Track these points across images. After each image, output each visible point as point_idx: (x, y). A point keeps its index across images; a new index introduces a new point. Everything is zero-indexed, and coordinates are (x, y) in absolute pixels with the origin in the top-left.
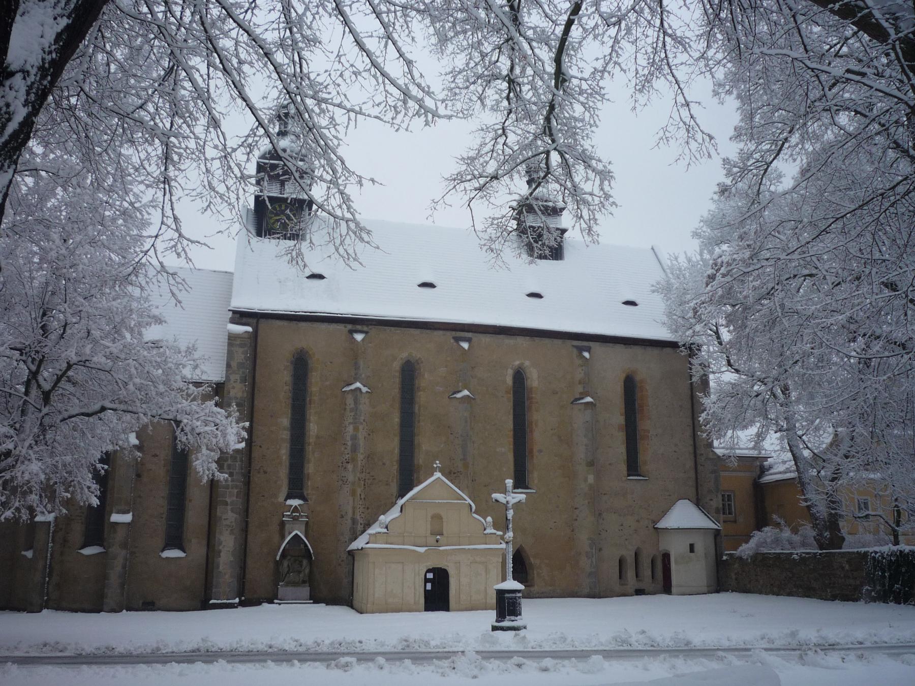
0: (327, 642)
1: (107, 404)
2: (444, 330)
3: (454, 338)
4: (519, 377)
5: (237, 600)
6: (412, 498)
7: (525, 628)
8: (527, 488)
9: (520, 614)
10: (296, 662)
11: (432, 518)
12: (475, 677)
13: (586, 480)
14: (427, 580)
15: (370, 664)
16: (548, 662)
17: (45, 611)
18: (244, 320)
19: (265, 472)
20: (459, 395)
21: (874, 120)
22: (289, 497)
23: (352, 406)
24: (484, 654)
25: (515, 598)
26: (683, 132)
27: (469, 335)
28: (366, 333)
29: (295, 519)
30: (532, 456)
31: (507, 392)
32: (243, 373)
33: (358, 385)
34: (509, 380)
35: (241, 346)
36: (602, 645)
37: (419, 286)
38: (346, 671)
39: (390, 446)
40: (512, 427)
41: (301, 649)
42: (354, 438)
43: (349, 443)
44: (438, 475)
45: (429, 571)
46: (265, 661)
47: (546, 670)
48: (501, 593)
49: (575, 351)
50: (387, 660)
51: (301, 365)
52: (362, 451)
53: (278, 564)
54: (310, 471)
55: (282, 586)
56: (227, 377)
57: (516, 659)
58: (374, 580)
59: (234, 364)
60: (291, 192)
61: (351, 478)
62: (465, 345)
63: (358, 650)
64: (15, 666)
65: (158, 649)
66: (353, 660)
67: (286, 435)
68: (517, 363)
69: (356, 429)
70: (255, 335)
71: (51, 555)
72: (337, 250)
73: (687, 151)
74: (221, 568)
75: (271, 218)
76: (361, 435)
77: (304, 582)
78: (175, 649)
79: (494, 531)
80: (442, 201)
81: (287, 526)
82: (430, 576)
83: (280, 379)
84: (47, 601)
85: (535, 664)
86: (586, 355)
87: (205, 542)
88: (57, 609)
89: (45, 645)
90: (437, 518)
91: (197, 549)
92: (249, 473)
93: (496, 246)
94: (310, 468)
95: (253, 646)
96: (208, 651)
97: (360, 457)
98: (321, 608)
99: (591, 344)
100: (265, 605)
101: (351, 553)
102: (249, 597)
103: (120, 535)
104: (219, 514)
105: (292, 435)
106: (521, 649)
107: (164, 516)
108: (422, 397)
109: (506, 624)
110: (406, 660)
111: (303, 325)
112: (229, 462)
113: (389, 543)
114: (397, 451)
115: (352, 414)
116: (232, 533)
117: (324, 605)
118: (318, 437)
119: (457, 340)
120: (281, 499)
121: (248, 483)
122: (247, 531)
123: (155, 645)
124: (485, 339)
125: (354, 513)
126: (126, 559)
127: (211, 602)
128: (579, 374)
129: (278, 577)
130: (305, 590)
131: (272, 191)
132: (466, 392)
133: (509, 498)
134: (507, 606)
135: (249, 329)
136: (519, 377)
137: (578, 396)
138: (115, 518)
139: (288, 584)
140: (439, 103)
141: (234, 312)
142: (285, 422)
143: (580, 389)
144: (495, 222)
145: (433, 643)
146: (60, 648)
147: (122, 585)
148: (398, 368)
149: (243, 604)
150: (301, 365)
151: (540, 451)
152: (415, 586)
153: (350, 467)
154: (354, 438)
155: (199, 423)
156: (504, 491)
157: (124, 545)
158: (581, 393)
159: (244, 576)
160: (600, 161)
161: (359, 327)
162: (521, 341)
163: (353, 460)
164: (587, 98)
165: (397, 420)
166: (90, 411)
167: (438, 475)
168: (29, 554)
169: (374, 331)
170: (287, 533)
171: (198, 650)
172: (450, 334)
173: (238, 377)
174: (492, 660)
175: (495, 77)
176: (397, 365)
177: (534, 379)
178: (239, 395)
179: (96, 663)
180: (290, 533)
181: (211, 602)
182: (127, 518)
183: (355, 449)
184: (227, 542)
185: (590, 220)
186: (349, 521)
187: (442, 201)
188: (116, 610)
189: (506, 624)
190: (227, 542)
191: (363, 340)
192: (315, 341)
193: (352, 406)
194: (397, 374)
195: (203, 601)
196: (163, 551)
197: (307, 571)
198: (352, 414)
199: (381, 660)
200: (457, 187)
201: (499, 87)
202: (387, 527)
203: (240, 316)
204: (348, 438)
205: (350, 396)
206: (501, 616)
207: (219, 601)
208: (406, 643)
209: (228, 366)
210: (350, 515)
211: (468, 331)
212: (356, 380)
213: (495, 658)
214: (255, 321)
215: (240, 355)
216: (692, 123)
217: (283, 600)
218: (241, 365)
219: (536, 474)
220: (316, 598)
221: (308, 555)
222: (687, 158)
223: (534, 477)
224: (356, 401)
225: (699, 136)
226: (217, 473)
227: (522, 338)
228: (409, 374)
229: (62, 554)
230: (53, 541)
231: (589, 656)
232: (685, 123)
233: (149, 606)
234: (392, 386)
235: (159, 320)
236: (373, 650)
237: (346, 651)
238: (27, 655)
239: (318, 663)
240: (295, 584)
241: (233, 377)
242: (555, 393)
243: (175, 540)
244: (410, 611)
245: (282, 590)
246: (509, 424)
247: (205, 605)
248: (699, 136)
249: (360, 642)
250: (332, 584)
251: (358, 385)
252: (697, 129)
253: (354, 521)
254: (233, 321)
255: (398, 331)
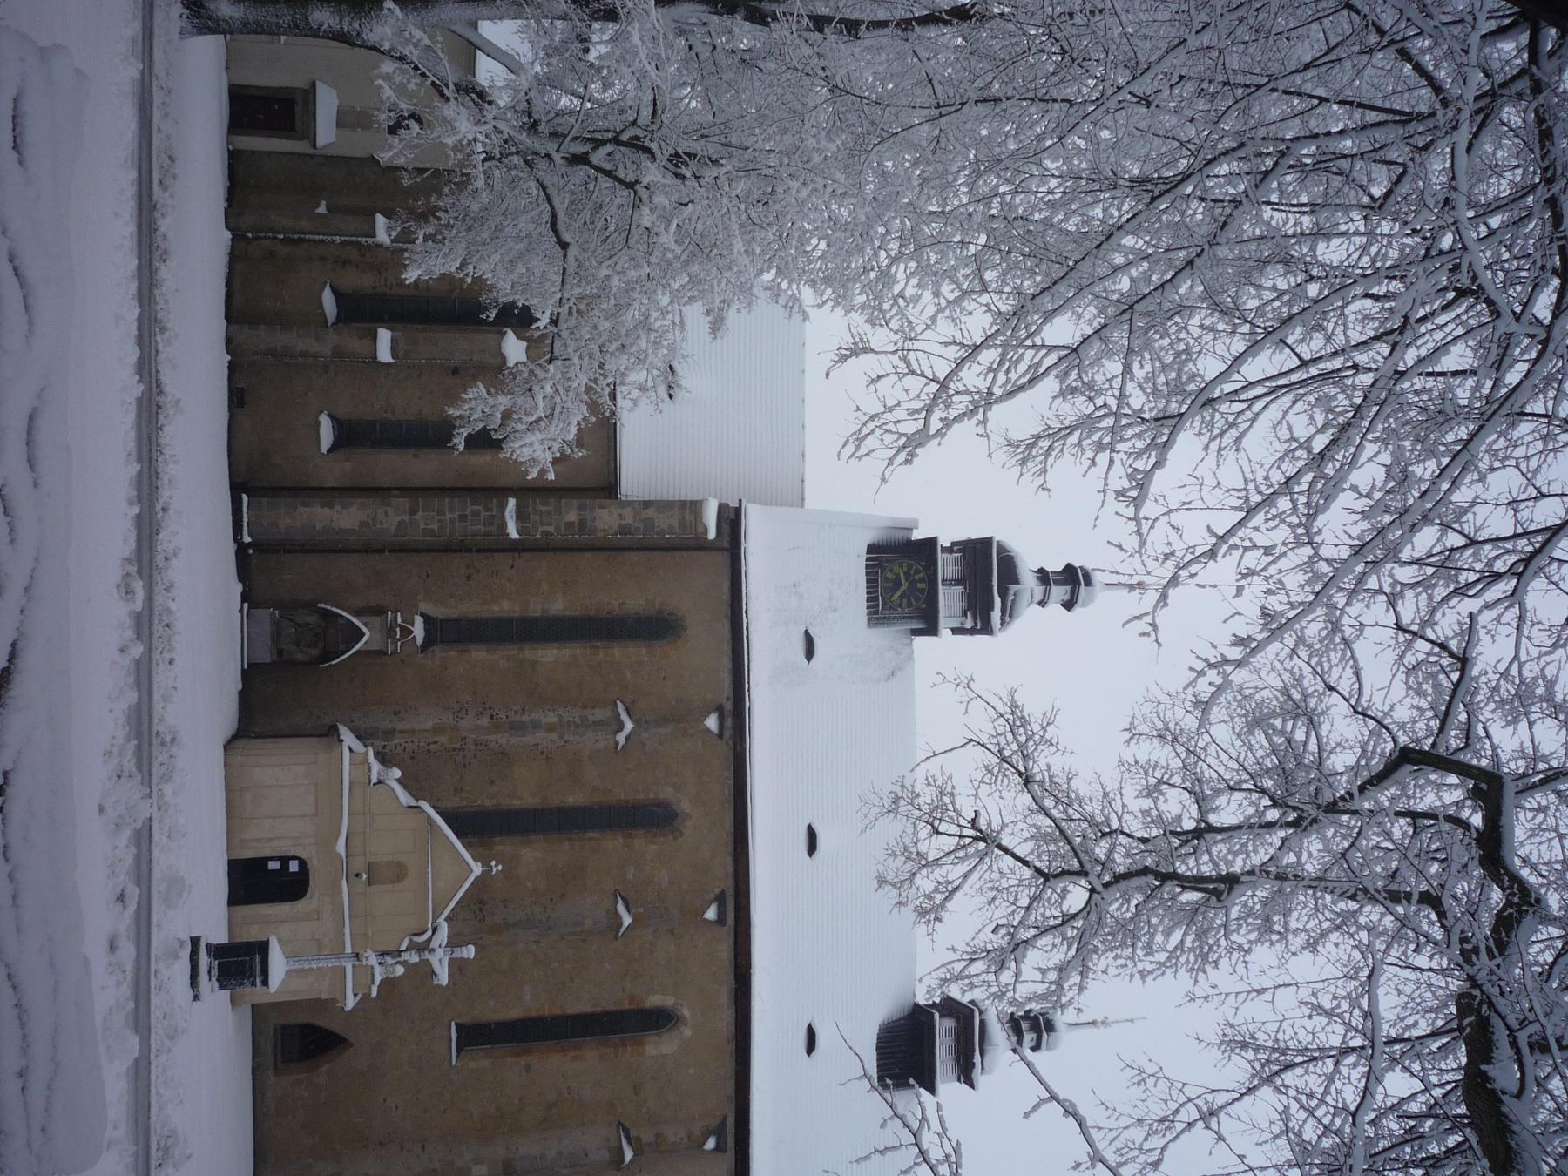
0: (173, 606)
1: (573, 252)
2: (736, 871)
3: (723, 892)
4: (661, 1020)
5: (247, 539)
6: (433, 823)
7: (196, 998)
8: (459, 1050)
9: (221, 987)
10: (136, 510)
11: (399, 864)
12: (101, 809)
13: (477, 1161)
14: (285, 860)
15: (130, 634)
16: (127, 951)
17: (228, 235)
18: (726, 528)
19: (469, 577)
20: (621, 908)
21: (1392, 42)
22: (428, 620)
23: (591, 719)
24: (146, 835)
25: (253, 975)
26: (1159, 1111)
27: (730, 921)
28: (720, 735)
29: (390, 632)
30: (518, 1055)
31: (632, 999)
32: (637, 529)
33: (629, 726)
34: (655, 1000)
35: (682, 523)
36: (161, 1109)
37: (810, 827)
38: (118, 587)
39: (524, 789)
40: (570, 1012)
41: (159, 559)
42: (536, 725)
43: (526, 718)
44: (477, 869)
45: (302, 863)
46: (139, 460)
47: (112, 947)
48: (263, 948)
49: (715, 1123)
50: (138, 662)
51: (657, 627)
52: (513, 741)
53: (311, 606)
54: (474, 654)
55: (272, 614)
56: (629, 503)
57: (133, 893)
58: (284, 769)
59: (650, 512)
60: (950, 600)
61: (466, 723)
62: (711, 914)
63: (156, 656)
64: (137, 75)
65: (163, 330)
66: (138, 604)
67: (535, 609)
68: (686, 1013)
69: (551, 728)
70: (701, 545)
71: (321, 241)
72: (872, 418)
73: (1125, 1121)
74: (301, 509)
75: (901, 566)
76: (541, 738)
77: (280, 653)
78: (162, 356)
79: (377, 982)
80: (972, 695)
81: (376, 620)
82: (294, 866)
83: (629, 593)
84: (244, 237)
85: (123, 930)
86: (711, 1144)
87: (347, 484)
88: (232, 254)
89: (170, 158)
90: (399, 872)
91: (337, 472)
92: (469, 550)
93: (903, 807)
94: (479, 654)
95: (166, 480)
96: (159, 407)
97: (503, 739)
98: (234, 683)
99: (731, 1153)
100: (239, 588)
101: (331, 732)
102: (254, 560)
103: (356, 345)
104: (395, 501)
105: (537, 620)
106: (153, 952)
107: (389, 416)
108: (613, 843)
109: (204, 959)
110: (136, 694)
111: (725, 627)
112: (483, 514)
113: (347, 793)
114: (517, 804)
115: (577, 720)
116: (363, 524)
117: (240, 687)
118: (534, 664)
119: (720, 900)
120: (424, 607)
121: (449, 549)
122: (366, 551)
123: (169, 325)
124: (725, 950)
125: (402, 732)
126: (316, 356)
127: (245, 497)
128: (674, 1134)
129: (288, 607)
130: (265, 656)
131: (946, 566)
132: (627, 920)
133: (440, 952)
134: (237, 963)
135: (712, 535)
136: (661, 1020)
137: (633, 1134)
138: (384, 336)
139: (276, 624)
140: (1148, 619)
141: (738, 511)
142: (558, 607)
143: (647, 1136)
144: (946, 799)
145: (168, 789)
146: (167, 181)
147: (272, 353)
148: (662, 796)
149: (241, 550)
150: (657, 627)
151: (528, 1068)
152: (276, 837)
153: (485, 721)
154: (536, 725)
155: (548, 390)
156: (454, 942)
157: (338, 353)
158: (638, 1138)
159: (289, 551)
160: (1081, 989)
161: (729, 722)
162: (727, 1016)
163: (497, 727)
164: (1191, 949)
165: (571, 800)
166: (561, 226)
167: (477, 869)
168: (322, 209)
169: (725, 749)
170: (365, 619)
171: (161, 393)
172: (728, 885)
173: (630, 520)
174: (133, 849)
175: (1200, 800)
176: (667, 793)
177: (661, 1047)
178: (599, 525)
179: (140, 227)
180: (365, 624)
181: (245, 497)
182: (384, 354)
183: (516, 728)
184: (347, 518)
185: (969, 977)
186: (387, 725)
187: (972, 695)
188: (230, 344)
189: (204, 959)
190: (347, 518)
191: (708, 730)
192: (703, 631)
193: (591, 719)
194: (652, 796)
195: (247, 481)
196: (331, 416)
197: (300, 657)
198: (577, 720)
199: (138, 650)
200: (1002, 721)
201: (1186, 815)
202: (379, 782)
203: (732, 520)
204: (534, 716)
205: (608, 713)
206: (217, 951)
207: (245, 510)
208: (168, 739)
209: (647, 504)
210: (400, 726)
211: (737, 918)
212: (636, 722)
213: (137, 859)
214: (726, 545)
215: (665, 522)
216: (1179, 1127)
217: (249, 618)
218: (649, 523)
219: (485, 1063)
220: (251, 674)
221: (327, 655)
222: (1112, 1124)
223: (481, 1061)
224: (599, 724)
225: (1156, 1142)
226: (465, 432)
227: (732, 1021)
228: (654, 817)
229: (323, 259)
230: (343, 243)
231: (137, 1032)
232: (1177, 1111)
233: (238, 398)
234: (626, 788)
235: (717, 326)
236: (156, 680)
237: (156, 635)
238: (155, 129)
239: (133, 544)
240: (276, 636)
241: (628, 512)
242: (637, 1089)
243: (347, 436)
244: (229, 832)
245: (265, 615)
246: (578, 1004)
247: (237, 488)
248: (1156, 1142)
249: (171, 662)
250: (282, 694)
251: (629, 726)
252: (1169, 1136)
253: (390, 734)
254: (722, 508)
255: (728, 792)
